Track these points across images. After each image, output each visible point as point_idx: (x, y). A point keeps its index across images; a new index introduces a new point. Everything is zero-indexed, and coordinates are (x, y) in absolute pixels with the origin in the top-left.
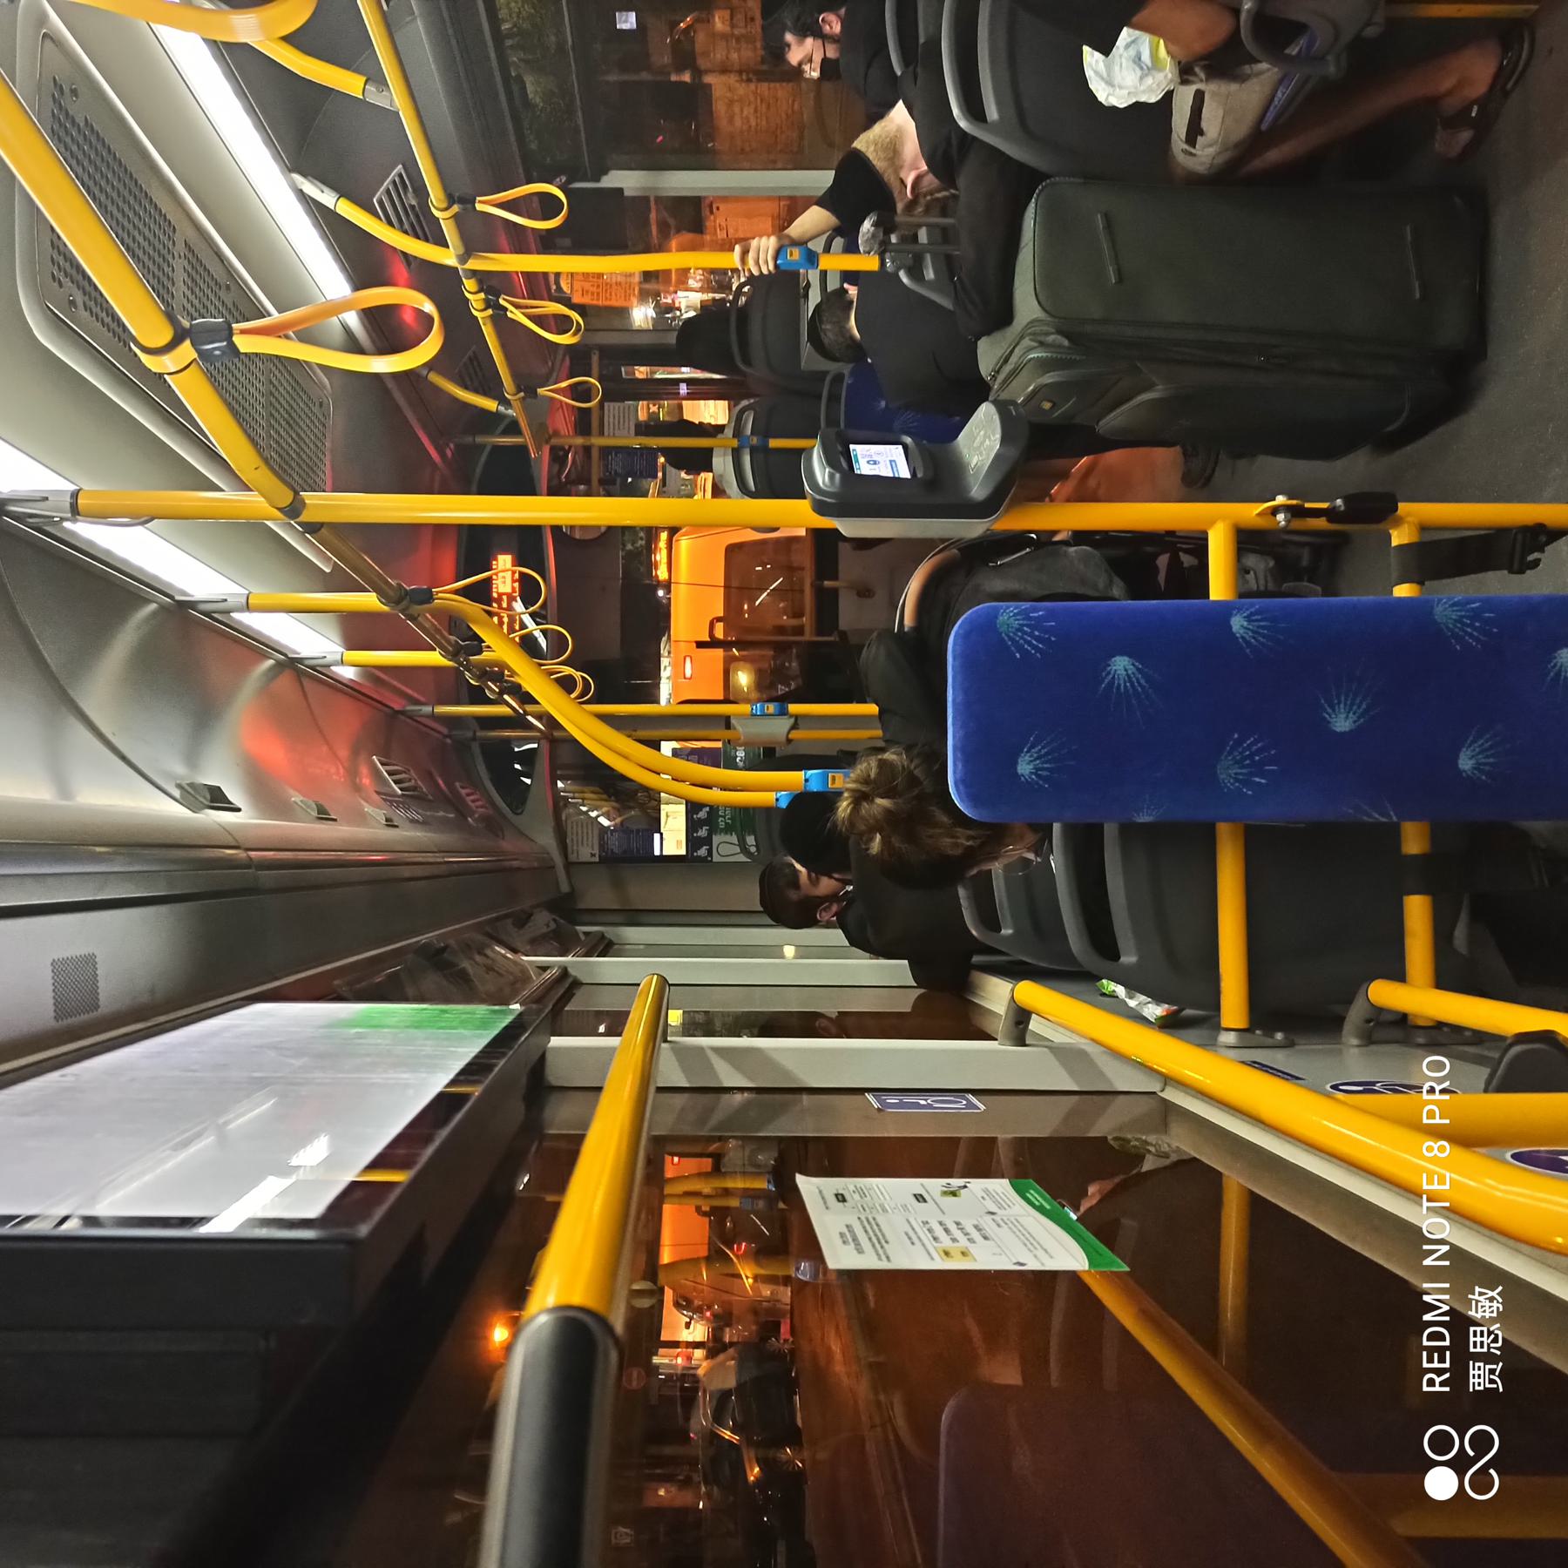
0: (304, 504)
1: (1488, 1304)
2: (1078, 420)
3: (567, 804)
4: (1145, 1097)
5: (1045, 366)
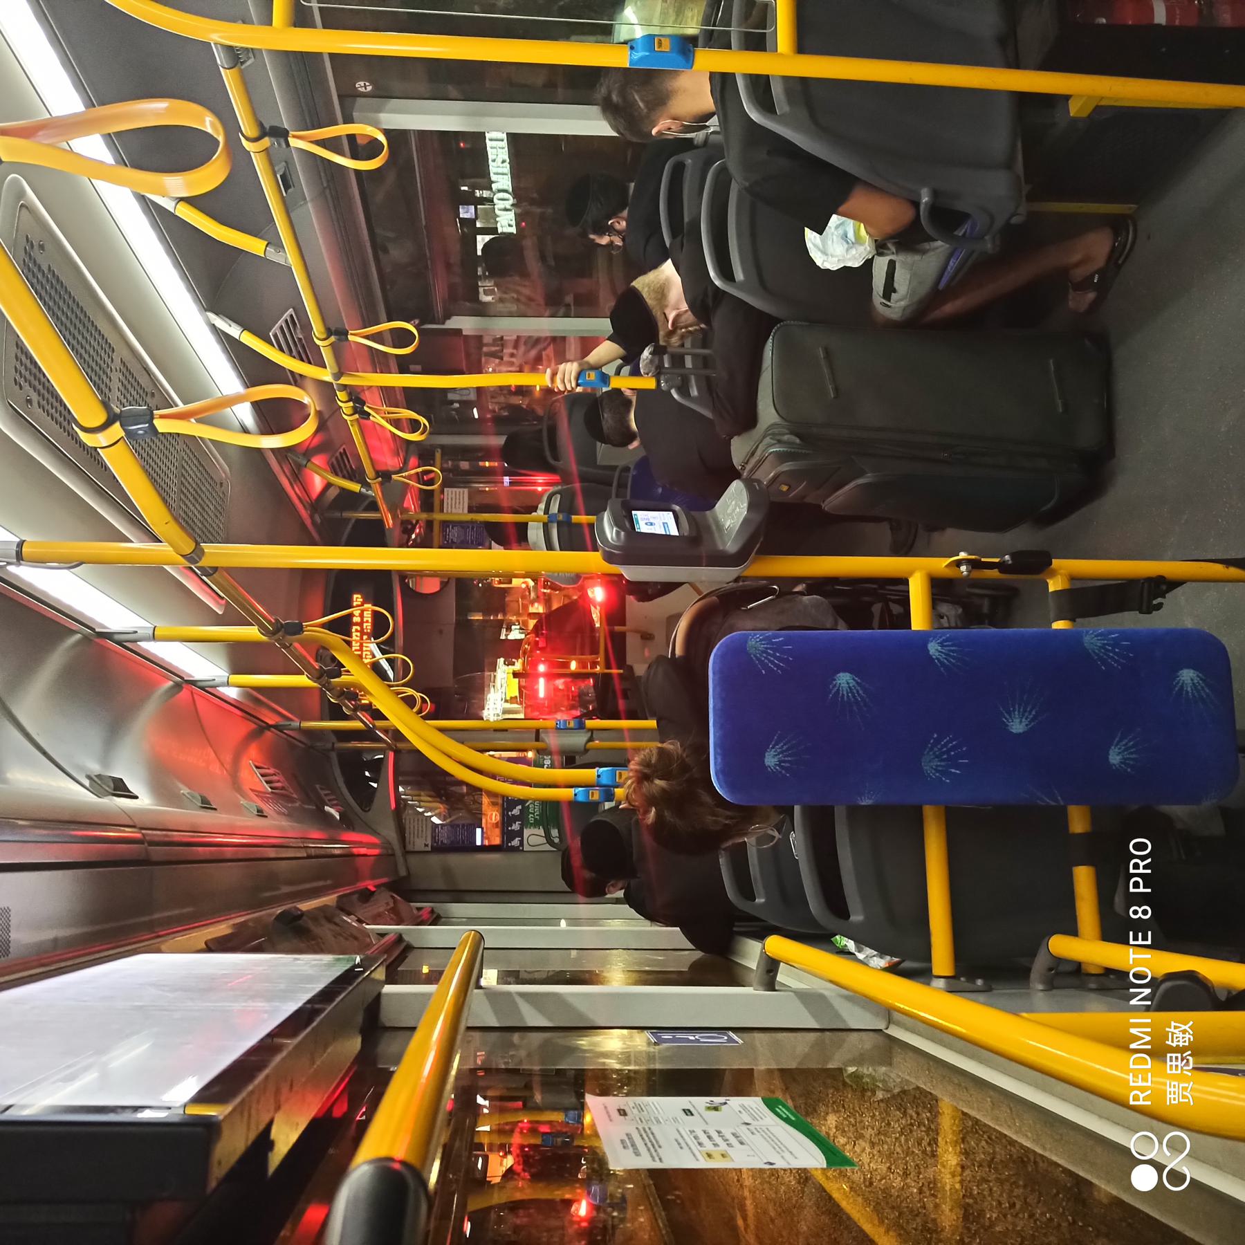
0: (203, 552)
1: (1181, 1035)
2: (808, 500)
3: (406, 805)
4: (871, 1034)
5: (782, 458)
